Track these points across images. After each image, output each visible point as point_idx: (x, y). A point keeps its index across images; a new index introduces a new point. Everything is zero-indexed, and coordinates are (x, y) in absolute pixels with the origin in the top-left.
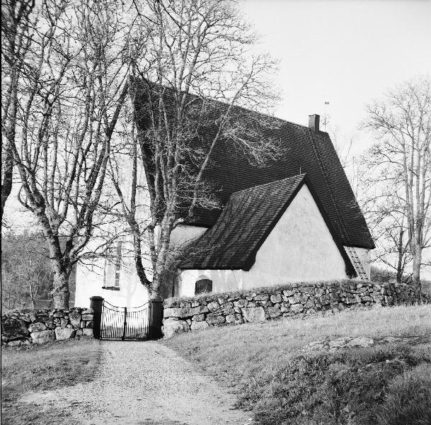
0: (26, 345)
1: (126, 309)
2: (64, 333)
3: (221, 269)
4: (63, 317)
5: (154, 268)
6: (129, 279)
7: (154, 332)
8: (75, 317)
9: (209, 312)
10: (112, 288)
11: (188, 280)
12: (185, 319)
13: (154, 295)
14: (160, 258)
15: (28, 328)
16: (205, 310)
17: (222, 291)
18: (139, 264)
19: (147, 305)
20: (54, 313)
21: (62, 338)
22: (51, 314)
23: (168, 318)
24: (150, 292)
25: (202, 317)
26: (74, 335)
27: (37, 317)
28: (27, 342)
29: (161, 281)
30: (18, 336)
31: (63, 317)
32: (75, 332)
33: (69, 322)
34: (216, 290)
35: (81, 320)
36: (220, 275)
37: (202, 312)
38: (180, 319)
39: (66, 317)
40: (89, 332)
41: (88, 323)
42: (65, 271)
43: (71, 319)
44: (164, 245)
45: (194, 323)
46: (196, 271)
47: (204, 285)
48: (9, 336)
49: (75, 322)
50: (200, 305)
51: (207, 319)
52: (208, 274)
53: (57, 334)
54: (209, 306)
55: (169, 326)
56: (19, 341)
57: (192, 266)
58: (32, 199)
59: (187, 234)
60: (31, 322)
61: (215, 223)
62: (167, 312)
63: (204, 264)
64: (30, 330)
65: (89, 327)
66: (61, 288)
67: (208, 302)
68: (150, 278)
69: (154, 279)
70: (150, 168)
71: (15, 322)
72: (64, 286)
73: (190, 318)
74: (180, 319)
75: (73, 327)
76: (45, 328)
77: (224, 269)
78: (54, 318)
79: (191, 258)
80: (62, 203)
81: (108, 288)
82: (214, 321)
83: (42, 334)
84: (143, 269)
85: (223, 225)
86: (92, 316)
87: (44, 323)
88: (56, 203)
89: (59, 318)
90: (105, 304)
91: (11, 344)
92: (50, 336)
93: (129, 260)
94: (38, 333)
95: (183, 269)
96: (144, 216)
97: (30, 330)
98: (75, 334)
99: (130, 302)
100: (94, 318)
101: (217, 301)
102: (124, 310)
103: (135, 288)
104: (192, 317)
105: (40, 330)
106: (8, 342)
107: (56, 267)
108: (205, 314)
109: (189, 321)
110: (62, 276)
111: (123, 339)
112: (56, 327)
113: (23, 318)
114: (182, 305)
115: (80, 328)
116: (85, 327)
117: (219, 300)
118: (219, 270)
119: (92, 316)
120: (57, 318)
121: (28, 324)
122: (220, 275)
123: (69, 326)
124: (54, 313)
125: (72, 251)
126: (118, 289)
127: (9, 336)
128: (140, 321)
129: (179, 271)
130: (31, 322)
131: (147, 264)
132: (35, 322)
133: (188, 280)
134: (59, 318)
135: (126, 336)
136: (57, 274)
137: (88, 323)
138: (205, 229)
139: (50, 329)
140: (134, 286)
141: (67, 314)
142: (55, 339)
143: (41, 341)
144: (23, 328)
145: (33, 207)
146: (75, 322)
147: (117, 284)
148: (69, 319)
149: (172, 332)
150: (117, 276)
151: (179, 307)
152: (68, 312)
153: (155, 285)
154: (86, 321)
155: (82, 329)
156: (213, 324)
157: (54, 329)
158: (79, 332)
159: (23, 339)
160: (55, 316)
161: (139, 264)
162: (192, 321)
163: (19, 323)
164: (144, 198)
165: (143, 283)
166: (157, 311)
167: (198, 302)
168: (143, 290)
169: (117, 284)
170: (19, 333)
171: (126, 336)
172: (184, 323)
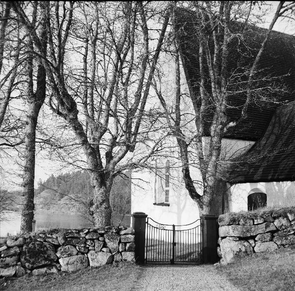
0: (53, 273)
1: (174, 226)
2: (99, 258)
3: (278, 180)
4: (98, 239)
5: (204, 179)
6: (179, 195)
7: (208, 254)
8: (112, 239)
9: (277, 230)
10: (162, 204)
11: (239, 196)
12: (246, 239)
13: (206, 211)
14: (210, 168)
15: (56, 252)
16: (272, 228)
17: (41, 229)
18: (187, 175)
19: (199, 223)
20: (86, 234)
21: (97, 265)
22: (82, 235)
23: (225, 237)
24: (201, 207)
25: (268, 236)
26: (111, 261)
27: (65, 238)
28: (54, 270)
29: (212, 194)
30: (43, 263)
31: (98, 239)
32: (112, 257)
33: (105, 245)
34: (270, 204)
35: (120, 242)
36: (277, 188)
37: (268, 230)
38: (240, 239)
39: (101, 239)
40: (129, 256)
41: (128, 245)
42: (105, 185)
43: (107, 241)
44: (214, 153)
45: (258, 243)
46: (248, 184)
47: (256, 200)
48: (33, 263)
49: (112, 245)
50: (265, 222)
51: (275, 239)
52: (262, 187)
53: (90, 259)
54: (276, 223)
55: (228, 248)
56: (45, 269)
57: (243, 179)
58: (62, 103)
59: (237, 147)
60: (59, 246)
61: (262, 136)
62: (223, 230)
63: (256, 177)
64: (58, 255)
65: (130, 250)
66: (101, 204)
67: (275, 218)
68: (200, 192)
69: (205, 192)
70: (192, 75)
71: (41, 245)
72: (104, 201)
73: (253, 238)
74: (240, 239)
75: (110, 252)
76: (75, 252)
77: (283, 180)
78: (87, 240)
79: (243, 172)
80: (104, 114)
81: (159, 204)
82: (284, 243)
83: (74, 258)
84: (192, 182)
85: (273, 137)
86: (133, 237)
87: (75, 247)
88: (96, 116)
89: (93, 240)
90: (150, 222)
91: (35, 272)
92: (82, 263)
93: (177, 174)
94: (67, 259)
95: (232, 184)
96: (191, 128)
97: (58, 255)
98: (113, 260)
99: (176, 218)
100: (135, 238)
101: (287, 217)
102: (171, 228)
103: (185, 203)
104: (256, 236)
105: (70, 255)
106: (32, 269)
107: (95, 181)
108: (272, 232)
109: (252, 242)
110: (102, 190)
111: (172, 263)
112: (89, 250)
113: (50, 240)
114: (242, 222)
115: (119, 252)
116: (125, 250)
117: (289, 215)
118: (275, 183)
119: (133, 237)
120: (90, 239)
121: (56, 247)
122: (277, 188)
123: (104, 249)
124: (86, 234)
125: (112, 162)
126: (169, 205)
127: (33, 263)
128: (191, 236)
129: (228, 185)
130: (59, 246)
131: (195, 174)
132: (63, 245)
133: (239, 196)
134: (93, 240)
135: (177, 259)
136: (96, 189)
137: (128, 245)
138: (253, 143)
139: (83, 254)
140: (184, 202)
141: (102, 235)
142: (89, 265)
143: (71, 269)
144: (51, 252)
145: (65, 112)
146: (112, 245)
147: (167, 201)
148: (104, 241)
149: (232, 256)
150: (167, 192)
151: (239, 224)
152: (103, 232)
153: (206, 199)
154: (125, 244)
155: (121, 253)
156: (283, 245)
157: (87, 254)
158: (118, 257)
159: (50, 266)
160: (87, 237)
161: (187, 175)
162: (255, 241)
163: (45, 246)
164: (188, 106)
165: (193, 197)
166: (210, 225)
167: (262, 217)
168: (192, 204)
169: (167, 201)
170: (46, 259)
171: (177, 259)
172: (246, 244)
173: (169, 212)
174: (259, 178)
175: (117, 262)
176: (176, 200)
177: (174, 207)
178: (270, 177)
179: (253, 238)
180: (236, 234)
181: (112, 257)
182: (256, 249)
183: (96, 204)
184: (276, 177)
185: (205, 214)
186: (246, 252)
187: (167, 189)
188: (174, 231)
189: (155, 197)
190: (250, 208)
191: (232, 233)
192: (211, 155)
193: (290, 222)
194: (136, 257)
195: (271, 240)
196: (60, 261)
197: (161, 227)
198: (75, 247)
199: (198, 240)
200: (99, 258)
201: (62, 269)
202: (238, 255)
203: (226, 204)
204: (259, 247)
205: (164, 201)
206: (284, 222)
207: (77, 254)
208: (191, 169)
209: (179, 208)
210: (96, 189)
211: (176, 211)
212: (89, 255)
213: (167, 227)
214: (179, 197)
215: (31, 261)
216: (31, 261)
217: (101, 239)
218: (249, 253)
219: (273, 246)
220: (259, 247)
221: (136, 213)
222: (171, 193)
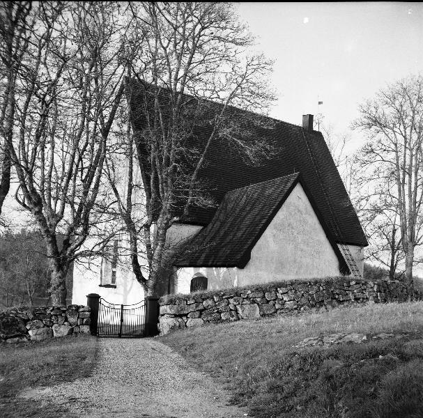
0: (24, 342)
1: (122, 306)
6: (126, 277)
8: (72, 315)
9: (205, 309)
11: (184, 278)
12: (181, 316)
16: (201, 307)
18: (135, 262)
19: (143, 303)
20: (52, 311)
21: (59, 335)
24: (146, 290)
28: (25, 339)
29: (157, 278)
32: (72, 329)
33: (66, 320)
35: (78, 318)
38: (176, 316)
39: (63, 315)
40: (86, 329)
41: (85, 320)
43: (68, 316)
47: (199, 283)
48: (7, 334)
49: (72, 320)
51: (203, 316)
52: (203, 271)
55: (165, 323)
58: (30, 199)
60: (29, 320)
62: (162, 309)
63: (200, 262)
65: (86, 324)
67: (203, 300)
68: (146, 275)
69: (150, 277)
72: (61, 283)
73: (186, 315)
75: (71, 325)
76: (42, 326)
78: (52, 316)
87: (42, 321)
90: (102, 302)
91: (9, 341)
93: (125, 258)
96: (140, 215)
97: (28, 327)
102: (120, 307)
105: (38, 328)
108: (201, 311)
109: (184, 318)
112: (53, 324)
115: (77, 325)
116: (82, 324)
117: (215, 297)
121: (26, 322)
122: (215, 273)
123: (66, 323)
124: (52, 311)
125: (69, 249)
126: (115, 287)
128: (136, 317)
129: (175, 269)
130: (29, 320)
131: (143, 261)
132: (33, 319)
135: (122, 332)
136: (54, 273)
137: (85, 320)
138: (201, 227)
139: (48, 326)
141: (64, 312)
143: (39, 338)
144: (21, 325)
147: (113, 281)
152: (65, 309)
153: (151, 283)
154: (83, 319)
158: (76, 330)
161: (135, 262)
162: (187, 318)
164: (140, 197)
165: (139, 280)
170: (18, 331)
172: (180, 320)
173: (115, 293)
174: (201, 263)
175: (76, 333)
176: (123, 281)
177: (120, 289)
178: (210, 263)
179: (186, 315)
180: (173, 312)
181: (72, 330)
182: (187, 324)
183: (53, 286)
184: (215, 263)
185: (148, 295)
186: (180, 326)
187: (114, 270)
188: (122, 309)
189: (101, 278)
190: (191, 291)
191: (169, 311)
192: (157, 244)
193: (215, 302)
194: (91, 330)
195: (200, 317)
196: (30, 332)
197: (112, 307)
198: (42, 321)
199: (142, 321)
200: (63, 330)
201: (31, 339)
202: (173, 329)
203: (171, 288)
204: (190, 322)
205: (110, 283)
206: (210, 302)
207: (44, 327)
208: (139, 259)
209: (125, 290)
210: (54, 273)
211: (122, 293)
212: (53, 328)
213: (116, 307)
214: (126, 278)
215: (6, 331)
216: (6, 331)
217: (63, 315)
218: (182, 327)
219: (200, 321)
220: (190, 322)
221: (92, 294)
222: (118, 275)
